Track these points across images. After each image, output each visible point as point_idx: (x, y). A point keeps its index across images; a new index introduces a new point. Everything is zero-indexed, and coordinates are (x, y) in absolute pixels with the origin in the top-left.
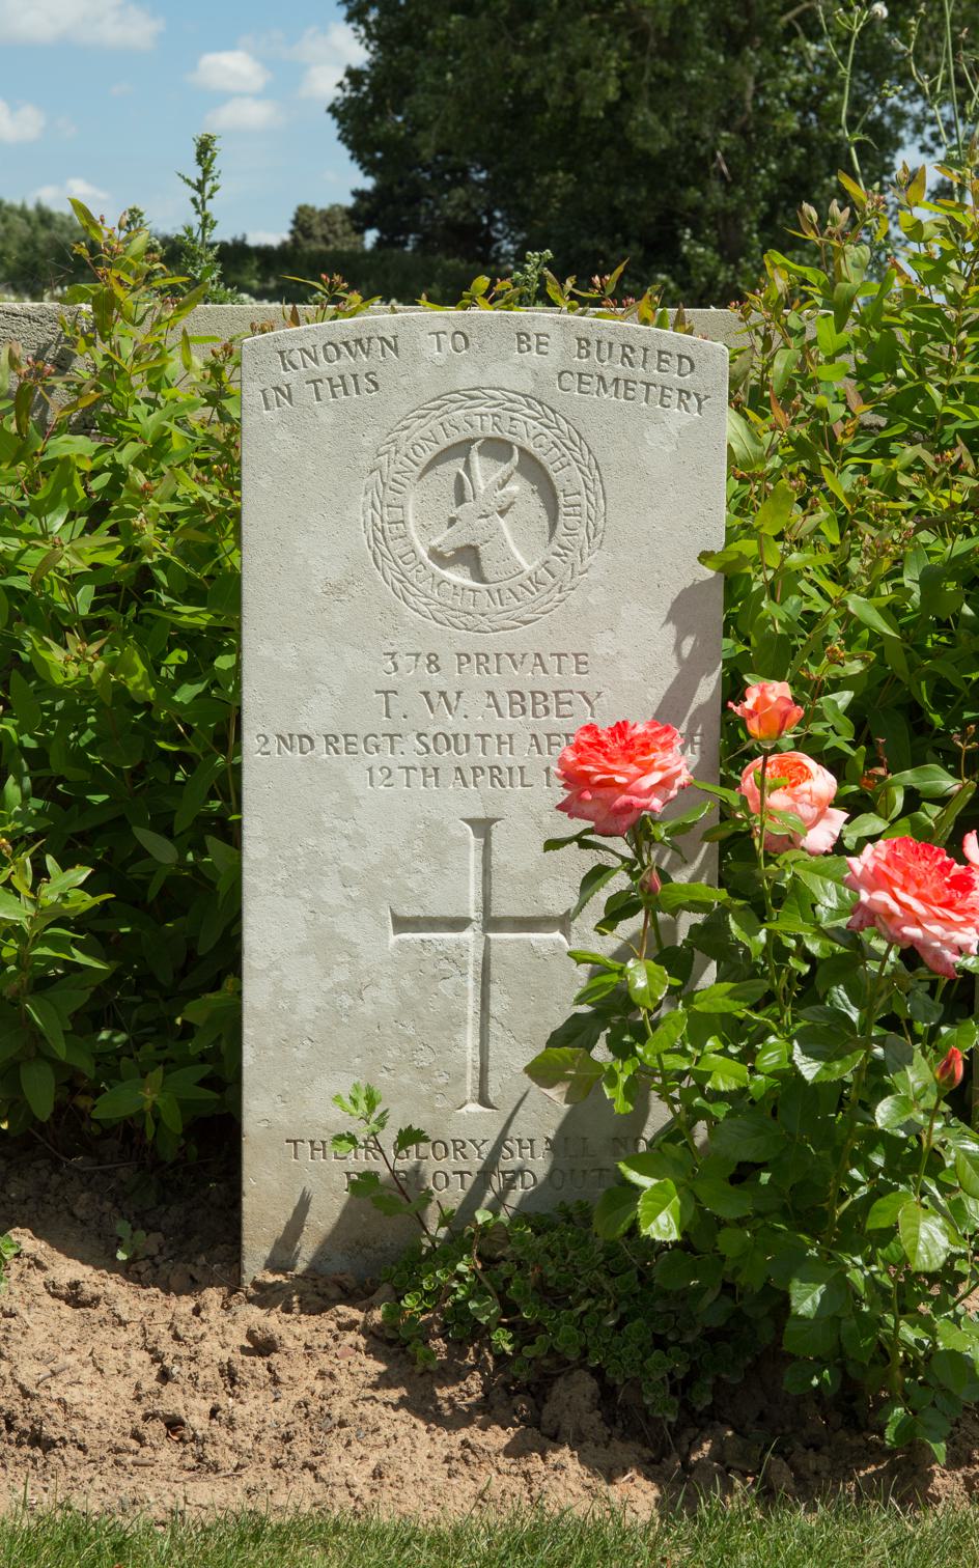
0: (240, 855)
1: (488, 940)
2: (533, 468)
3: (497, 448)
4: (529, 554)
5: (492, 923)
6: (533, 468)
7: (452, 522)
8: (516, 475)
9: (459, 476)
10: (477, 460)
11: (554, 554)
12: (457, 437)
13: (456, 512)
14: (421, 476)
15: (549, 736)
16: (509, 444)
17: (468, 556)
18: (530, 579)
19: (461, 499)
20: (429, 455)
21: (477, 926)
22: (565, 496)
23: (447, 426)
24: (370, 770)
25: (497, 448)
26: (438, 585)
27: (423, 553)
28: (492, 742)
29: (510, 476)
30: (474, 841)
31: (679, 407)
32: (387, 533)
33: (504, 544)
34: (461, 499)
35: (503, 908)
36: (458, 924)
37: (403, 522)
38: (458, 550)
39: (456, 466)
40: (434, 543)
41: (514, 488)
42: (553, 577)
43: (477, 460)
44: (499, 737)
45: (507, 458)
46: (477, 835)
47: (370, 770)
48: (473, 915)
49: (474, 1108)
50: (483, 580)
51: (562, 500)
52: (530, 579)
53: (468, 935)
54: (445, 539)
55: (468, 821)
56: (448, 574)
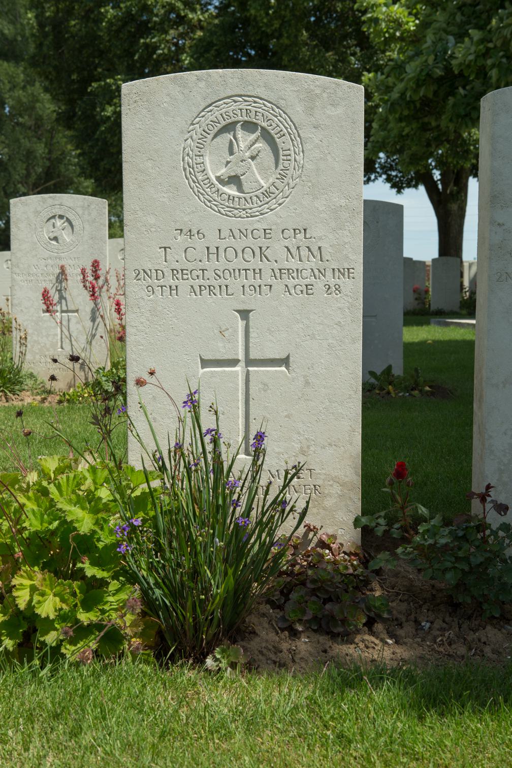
0: (467, 422)
1: (248, 371)
2: (68, 220)
3: (61, 217)
4: (266, 178)
5: (249, 362)
6: (267, 136)
7: (228, 163)
8: (261, 140)
9: (231, 141)
10: (240, 133)
11: (277, 179)
12: (53, 214)
13: (53, 230)
14: (213, 139)
15: (280, 270)
16: (256, 125)
17: (234, 180)
18: (266, 191)
19: (231, 152)
20: (216, 129)
21: (242, 363)
22: (283, 151)
23: (224, 115)
24: (243, 287)
25: (249, 126)
26: (221, 196)
27: (47, 238)
28: (251, 273)
29: (258, 139)
30: (241, 324)
31: (289, 279)
32: (196, 169)
33: (254, 173)
34: (231, 152)
35: (252, 356)
36: (234, 362)
37: (203, 163)
38: (229, 177)
39: (53, 221)
40: (218, 175)
41: (65, 224)
42: (278, 189)
43: (240, 133)
44: (254, 270)
45: (253, 132)
46: (242, 319)
47: (243, 287)
48: (240, 358)
49: (60, 350)
50: (243, 192)
51: (281, 152)
52: (266, 191)
53: (239, 369)
54: (223, 171)
55: (238, 311)
56: (226, 189)
